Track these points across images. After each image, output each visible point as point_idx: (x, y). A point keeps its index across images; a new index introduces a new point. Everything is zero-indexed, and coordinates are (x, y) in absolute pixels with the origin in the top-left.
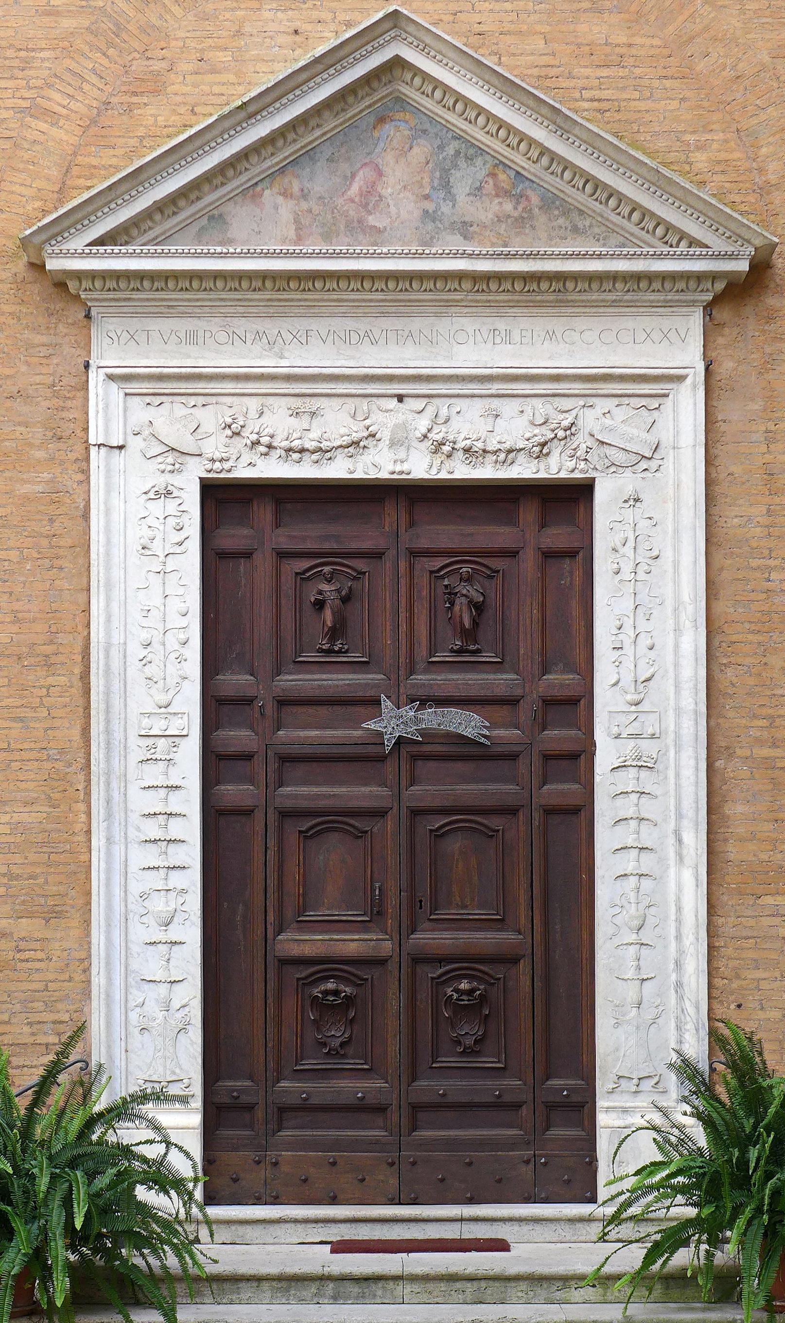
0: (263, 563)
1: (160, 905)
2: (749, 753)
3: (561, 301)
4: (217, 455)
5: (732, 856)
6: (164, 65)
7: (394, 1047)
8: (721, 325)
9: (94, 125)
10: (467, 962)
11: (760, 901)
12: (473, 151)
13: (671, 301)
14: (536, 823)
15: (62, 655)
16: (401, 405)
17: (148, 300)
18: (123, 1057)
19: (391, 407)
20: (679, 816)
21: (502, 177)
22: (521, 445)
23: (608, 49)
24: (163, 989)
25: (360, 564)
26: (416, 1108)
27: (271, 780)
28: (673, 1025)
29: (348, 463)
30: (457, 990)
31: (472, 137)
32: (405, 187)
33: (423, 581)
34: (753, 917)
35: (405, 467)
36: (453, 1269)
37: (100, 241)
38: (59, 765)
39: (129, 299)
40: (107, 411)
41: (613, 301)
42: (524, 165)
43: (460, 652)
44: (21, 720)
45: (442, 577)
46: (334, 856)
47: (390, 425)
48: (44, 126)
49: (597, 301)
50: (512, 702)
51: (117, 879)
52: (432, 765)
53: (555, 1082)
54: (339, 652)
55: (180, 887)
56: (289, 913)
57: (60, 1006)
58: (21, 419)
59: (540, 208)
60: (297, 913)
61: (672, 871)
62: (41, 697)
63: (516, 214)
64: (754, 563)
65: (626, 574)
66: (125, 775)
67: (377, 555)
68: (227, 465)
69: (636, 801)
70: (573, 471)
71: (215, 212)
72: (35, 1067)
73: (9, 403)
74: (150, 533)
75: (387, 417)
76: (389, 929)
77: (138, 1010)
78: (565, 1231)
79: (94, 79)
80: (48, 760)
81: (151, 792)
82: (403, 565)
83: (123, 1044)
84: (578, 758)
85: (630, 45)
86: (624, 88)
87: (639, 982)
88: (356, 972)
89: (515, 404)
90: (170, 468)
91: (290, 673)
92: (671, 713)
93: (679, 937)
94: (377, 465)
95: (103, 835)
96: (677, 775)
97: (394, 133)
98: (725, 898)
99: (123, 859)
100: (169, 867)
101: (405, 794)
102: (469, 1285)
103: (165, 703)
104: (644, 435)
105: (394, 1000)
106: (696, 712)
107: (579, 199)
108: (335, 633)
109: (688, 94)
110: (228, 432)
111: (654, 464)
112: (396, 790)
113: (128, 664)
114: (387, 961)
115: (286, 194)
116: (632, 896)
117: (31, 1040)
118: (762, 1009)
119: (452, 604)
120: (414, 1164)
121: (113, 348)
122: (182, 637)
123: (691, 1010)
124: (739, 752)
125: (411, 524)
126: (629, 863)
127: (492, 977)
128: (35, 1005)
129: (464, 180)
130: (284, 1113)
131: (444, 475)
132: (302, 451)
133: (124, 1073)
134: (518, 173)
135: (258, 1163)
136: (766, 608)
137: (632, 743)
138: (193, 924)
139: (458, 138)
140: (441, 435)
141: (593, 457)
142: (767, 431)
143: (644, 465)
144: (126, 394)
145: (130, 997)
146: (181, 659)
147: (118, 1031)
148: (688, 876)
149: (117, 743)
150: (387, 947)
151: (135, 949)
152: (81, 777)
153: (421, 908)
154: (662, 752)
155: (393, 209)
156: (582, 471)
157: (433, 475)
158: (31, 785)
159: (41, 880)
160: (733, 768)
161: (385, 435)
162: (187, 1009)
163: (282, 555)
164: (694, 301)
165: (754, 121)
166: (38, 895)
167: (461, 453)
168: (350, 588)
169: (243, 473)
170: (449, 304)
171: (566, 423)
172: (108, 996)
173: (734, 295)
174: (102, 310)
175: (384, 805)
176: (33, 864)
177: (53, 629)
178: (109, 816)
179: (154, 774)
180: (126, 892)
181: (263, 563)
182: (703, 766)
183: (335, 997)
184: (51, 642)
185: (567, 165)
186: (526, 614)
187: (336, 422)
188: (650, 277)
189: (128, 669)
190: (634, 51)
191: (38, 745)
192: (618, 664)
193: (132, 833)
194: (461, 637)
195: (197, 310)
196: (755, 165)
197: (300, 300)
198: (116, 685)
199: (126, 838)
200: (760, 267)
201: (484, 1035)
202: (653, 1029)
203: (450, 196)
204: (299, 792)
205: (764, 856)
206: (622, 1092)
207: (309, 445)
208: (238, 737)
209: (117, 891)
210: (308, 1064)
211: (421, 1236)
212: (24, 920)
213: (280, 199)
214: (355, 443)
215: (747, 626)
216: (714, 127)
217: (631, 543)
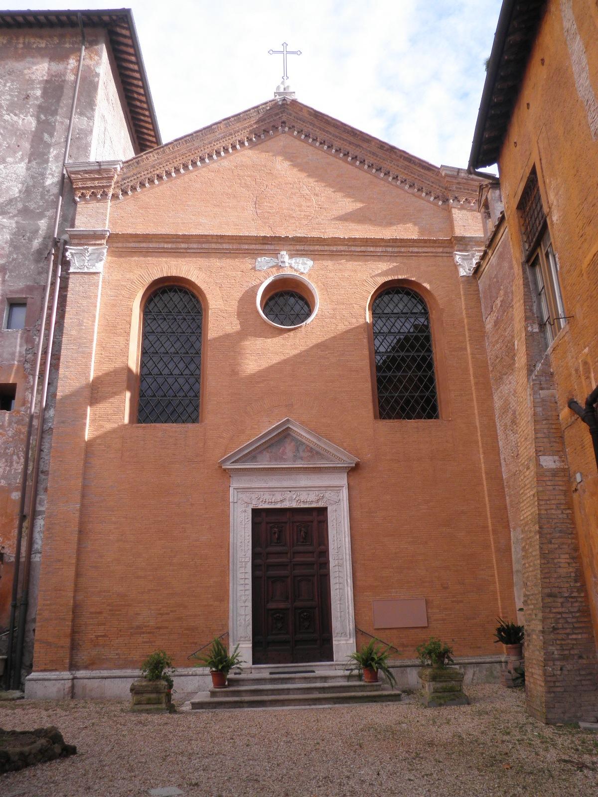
1: (243, 598)
15: (223, 545)
20: (347, 576)
25: (283, 524)
37: (233, 462)
40: (233, 495)
50: (313, 552)
67: (286, 523)
75: (288, 495)
84: (326, 564)
93: (348, 602)
94: (286, 505)
108: (278, 539)
115: (268, 452)
121: (235, 484)
123: (351, 617)
146: (248, 546)
147: (235, 626)
148: (349, 588)
154: (343, 563)
163: (267, 523)
169: (260, 507)
173: (354, 470)
179: (242, 570)
188: (337, 467)
198: (235, 551)
200: (357, 465)
203: (299, 452)
204: (271, 573)
211: (297, 670)
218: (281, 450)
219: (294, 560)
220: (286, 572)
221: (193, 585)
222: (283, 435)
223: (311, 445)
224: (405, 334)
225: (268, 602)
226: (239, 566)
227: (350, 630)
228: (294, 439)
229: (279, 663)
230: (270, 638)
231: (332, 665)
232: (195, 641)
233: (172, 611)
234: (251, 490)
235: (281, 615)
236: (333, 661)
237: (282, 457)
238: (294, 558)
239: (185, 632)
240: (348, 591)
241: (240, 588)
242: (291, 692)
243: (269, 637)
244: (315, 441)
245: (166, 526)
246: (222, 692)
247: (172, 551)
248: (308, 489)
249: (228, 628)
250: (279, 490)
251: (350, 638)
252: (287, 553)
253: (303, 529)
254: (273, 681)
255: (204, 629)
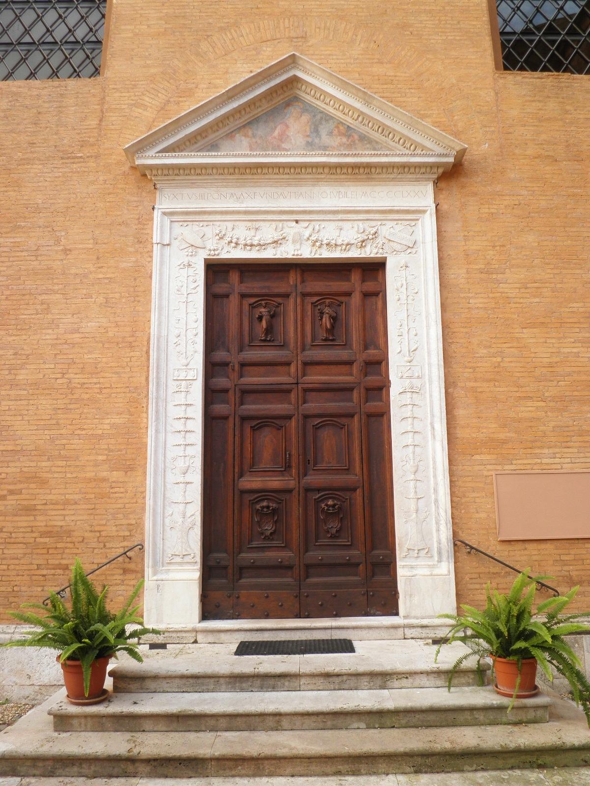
0: (234, 300)
1: (181, 464)
2: (464, 385)
3: (369, 178)
4: (212, 248)
5: (459, 436)
6: (194, 86)
7: (296, 534)
8: (441, 190)
9: (163, 109)
10: (331, 491)
11: (473, 458)
12: (328, 118)
13: (419, 178)
14: (363, 421)
15: (134, 341)
16: (297, 225)
17: (183, 180)
18: (161, 543)
19: (292, 226)
20: (433, 416)
21: (341, 128)
22: (352, 242)
23: (386, 77)
24: (181, 507)
25: (279, 300)
26: (308, 566)
27: (237, 402)
28: (434, 522)
29: (274, 251)
30: (327, 505)
31: (328, 111)
32: (298, 132)
33: (309, 307)
34: (470, 466)
35: (299, 252)
36: (330, 669)
38: (135, 395)
39: (174, 180)
41: (393, 178)
42: (350, 121)
43: (326, 340)
44: (117, 373)
45: (317, 306)
46: (267, 439)
47: (292, 234)
48: (140, 111)
49: (385, 178)
50: (350, 363)
51: (161, 451)
52: (314, 394)
53: (376, 552)
54: (270, 341)
55: (191, 455)
56: (246, 467)
57: (131, 516)
58: (124, 234)
59: (359, 140)
60: (253, 467)
61: (430, 443)
62: (127, 362)
63: (348, 143)
64: (462, 295)
65: (403, 301)
66: (166, 399)
67: (286, 296)
68: (216, 252)
69: (411, 409)
70: (376, 254)
71: (214, 143)
72: (118, 548)
73: (118, 227)
74: (181, 284)
75: (291, 230)
76: (294, 475)
77: (169, 517)
78: (383, 634)
79: (163, 92)
80: (129, 393)
81: (178, 407)
82: (299, 300)
83: (161, 535)
85: (395, 76)
86: (394, 93)
87: (415, 500)
88: (277, 496)
89: (349, 224)
90: (190, 254)
91: (247, 351)
92: (426, 366)
93: (435, 476)
94: (287, 252)
95: (154, 428)
96: (431, 396)
97: (293, 111)
98: (456, 456)
99: (164, 440)
100: (186, 445)
101: (300, 410)
102: (337, 679)
103: (186, 364)
104: (409, 237)
105: (296, 510)
106: (438, 365)
107: (376, 136)
108: (269, 330)
109: (422, 95)
110: (217, 237)
111: (414, 250)
112: (296, 406)
113: (169, 345)
114: (292, 490)
115: (246, 136)
116: (411, 456)
117: (115, 534)
118: (477, 512)
119: (322, 318)
120: (307, 596)
122: (195, 332)
124: (459, 384)
125: (303, 281)
126: (409, 439)
127: (343, 498)
128: (118, 516)
129: (324, 131)
130: (242, 570)
131: (317, 256)
132: (252, 245)
133: (161, 550)
134: (348, 126)
135: (229, 597)
136: (468, 316)
137: (408, 381)
138: (197, 473)
139: (322, 112)
140: (316, 238)
141: (386, 247)
142: (464, 236)
143: (409, 251)
144: (172, 221)
145: (166, 511)
146: (194, 343)
147: (159, 528)
149: (162, 383)
150: (292, 484)
151: (168, 486)
152: (145, 400)
153: (309, 464)
155: (293, 141)
156: (381, 254)
157: (312, 256)
158: (121, 405)
159: (124, 452)
160: (458, 393)
161: (290, 238)
162: (193, 517)
163: (243, 296)
164: (429, 178)
165: (451, 106)
166: (122, 460)
167: (325, 245)
168: (275, 311)
169: (224, 255)
170: (319, 180)
171: (372, 232)
172: (154, 510)
173: (450, 174)
174: (161, 185)
175: (291, 413)
176: (119, 444)
177: (134, 329)
178: (157, 419)
179: (181, 398)
180: (165, 457)
181: (234, 300)
182: (443, 391)
183: (271, 507)
184: (133, 336)
185: (371, 119)
186: (355, 323)
187: (268, 233)
189: (169, 348)
190: (397, 78)
191: (125, 385)
192: (401, 343)
193: (169, 428)
194: (326, 333)
195: (205, 184)
196: (452, 123)
197: (251, 179)
198: (163, 356)
199: (166, 430)
201: (341, 528)
202: (424, 524)
204: (252, 407)
205: (474, 435)
206: (410, 557)
207: (255, 243)
208: (221, 382)
209: (161, 457)
210: (255, 544)
212: (115, 472)
213: (243, 138)
214: (275, 242)
215: (460, 324)
216: (434, 108)
217: (405, 287)
218: (276, 133)
219: (307, 379)
220: (286, 406)
221: (63, 431)
222: (280, 95)
223: (349, 120)
224: (514, 38)
225: (241, 475)
226: (171, 390)
227: (439, 543)
228: (308, 108)
229: (267, 616)
230: (248, 557)
231: (395, 627)
232: (64, 562)
233: (11, 492)
234: (206, 217)
235: (273, 505)
236: (397, 614)
237: (279, 146)
238: (304, 375)
239: (42, 540)
240: (434, 452)
241: (173, 439)
242: (285, 722)
243: (243, 555)
244: (358, 105)
245: (7, 299)
246: (86, 716)
247: (15, 354)
248: (340, 216)
249: (143, 534)
250: (269, 217)
251: (440, 561)
252: (288, 364)
253: (327, 310)
254: (238, 681)
255: (87, 535)
